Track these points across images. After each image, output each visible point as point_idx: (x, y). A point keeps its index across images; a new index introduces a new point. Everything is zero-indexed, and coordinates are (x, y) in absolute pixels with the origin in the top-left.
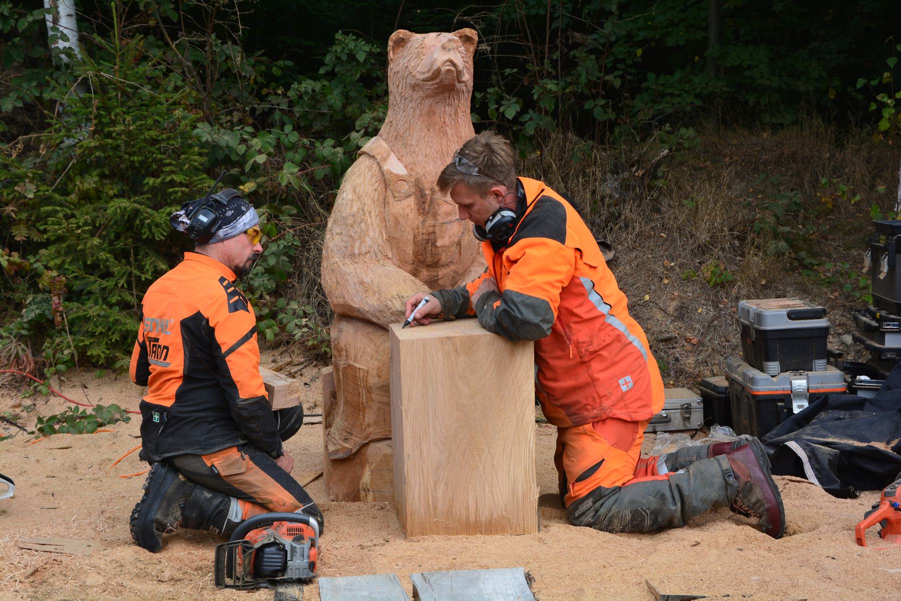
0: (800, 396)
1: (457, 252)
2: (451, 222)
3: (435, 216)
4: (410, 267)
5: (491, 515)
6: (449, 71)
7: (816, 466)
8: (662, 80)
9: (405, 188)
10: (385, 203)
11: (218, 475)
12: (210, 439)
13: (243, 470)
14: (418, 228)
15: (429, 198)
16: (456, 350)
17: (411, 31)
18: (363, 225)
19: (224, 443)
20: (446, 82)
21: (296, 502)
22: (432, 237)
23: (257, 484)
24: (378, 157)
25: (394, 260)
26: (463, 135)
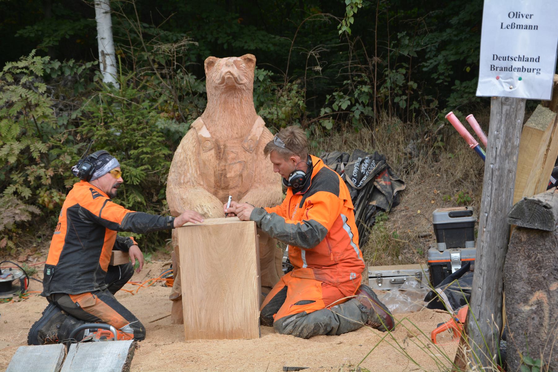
0: (456, 263)
1: (240, 180)
2: (235, 163)
3: (226, 160)
4: (213, 190)
5: (232, 328)
6: (229, 78)
7: (453, 303)
8: (464, 84)
9: (209, 144)
10: (199, 154)
11: (80, 307)
12: (77, 286)
13: (94, 304)
14: (216, 167)
15: (222, 150)
16: (210, 233)
17: (217, 57)
18: (186, 167)
19: (85, 289)
20: (230, 84)
21: (125, 320)
22: (224, 172)
23: (101, 311)
24: (197, 128)
25: (205, 186)
26: (246, 114)
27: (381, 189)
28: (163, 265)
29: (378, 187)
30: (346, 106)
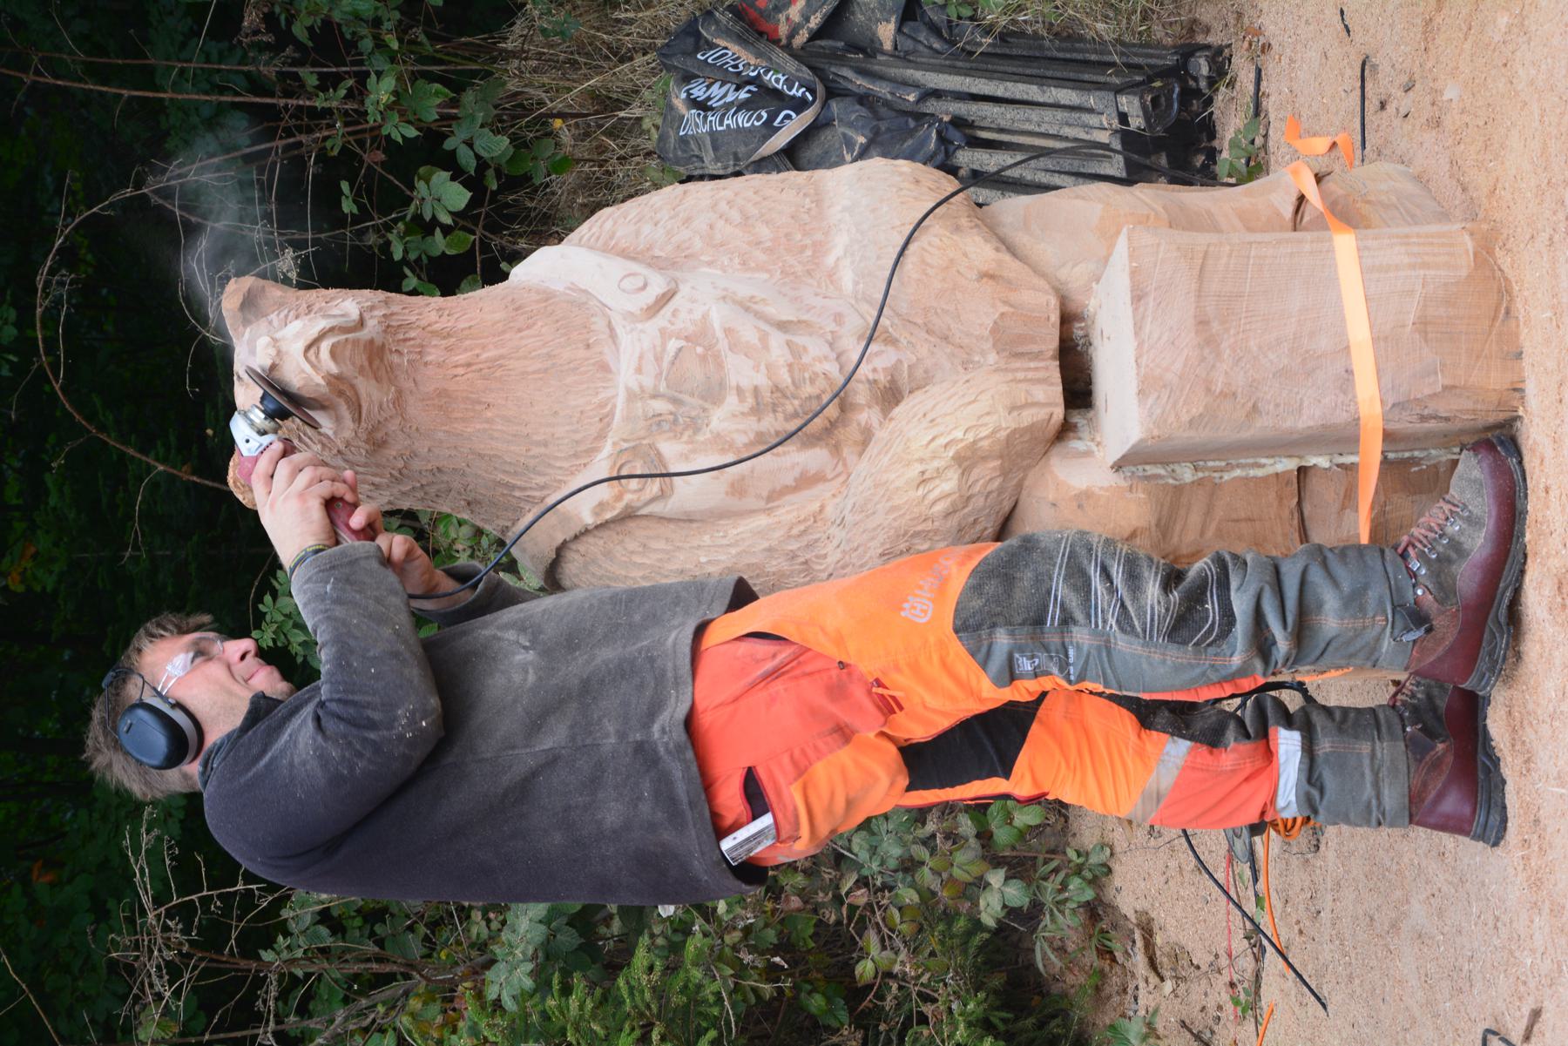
6: (333, 354)
27: (826, 9)
28: (1153, 979)
29: (815, 21)
30: (457, 187)
